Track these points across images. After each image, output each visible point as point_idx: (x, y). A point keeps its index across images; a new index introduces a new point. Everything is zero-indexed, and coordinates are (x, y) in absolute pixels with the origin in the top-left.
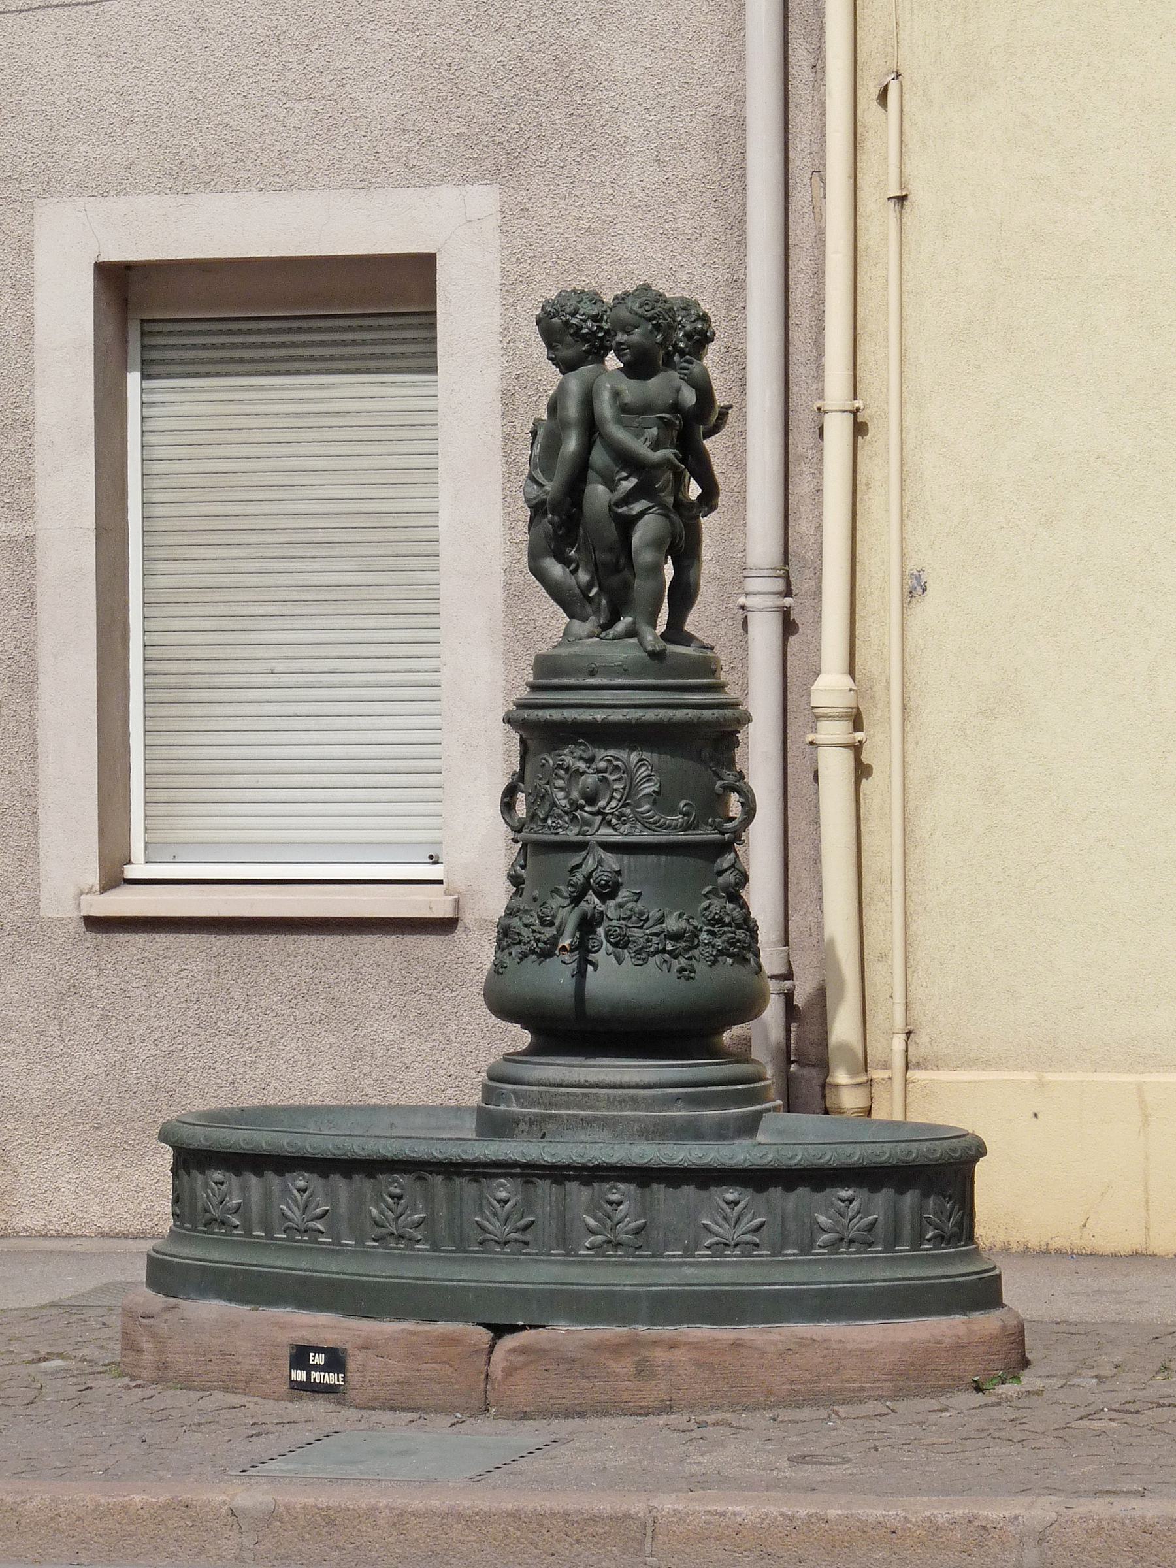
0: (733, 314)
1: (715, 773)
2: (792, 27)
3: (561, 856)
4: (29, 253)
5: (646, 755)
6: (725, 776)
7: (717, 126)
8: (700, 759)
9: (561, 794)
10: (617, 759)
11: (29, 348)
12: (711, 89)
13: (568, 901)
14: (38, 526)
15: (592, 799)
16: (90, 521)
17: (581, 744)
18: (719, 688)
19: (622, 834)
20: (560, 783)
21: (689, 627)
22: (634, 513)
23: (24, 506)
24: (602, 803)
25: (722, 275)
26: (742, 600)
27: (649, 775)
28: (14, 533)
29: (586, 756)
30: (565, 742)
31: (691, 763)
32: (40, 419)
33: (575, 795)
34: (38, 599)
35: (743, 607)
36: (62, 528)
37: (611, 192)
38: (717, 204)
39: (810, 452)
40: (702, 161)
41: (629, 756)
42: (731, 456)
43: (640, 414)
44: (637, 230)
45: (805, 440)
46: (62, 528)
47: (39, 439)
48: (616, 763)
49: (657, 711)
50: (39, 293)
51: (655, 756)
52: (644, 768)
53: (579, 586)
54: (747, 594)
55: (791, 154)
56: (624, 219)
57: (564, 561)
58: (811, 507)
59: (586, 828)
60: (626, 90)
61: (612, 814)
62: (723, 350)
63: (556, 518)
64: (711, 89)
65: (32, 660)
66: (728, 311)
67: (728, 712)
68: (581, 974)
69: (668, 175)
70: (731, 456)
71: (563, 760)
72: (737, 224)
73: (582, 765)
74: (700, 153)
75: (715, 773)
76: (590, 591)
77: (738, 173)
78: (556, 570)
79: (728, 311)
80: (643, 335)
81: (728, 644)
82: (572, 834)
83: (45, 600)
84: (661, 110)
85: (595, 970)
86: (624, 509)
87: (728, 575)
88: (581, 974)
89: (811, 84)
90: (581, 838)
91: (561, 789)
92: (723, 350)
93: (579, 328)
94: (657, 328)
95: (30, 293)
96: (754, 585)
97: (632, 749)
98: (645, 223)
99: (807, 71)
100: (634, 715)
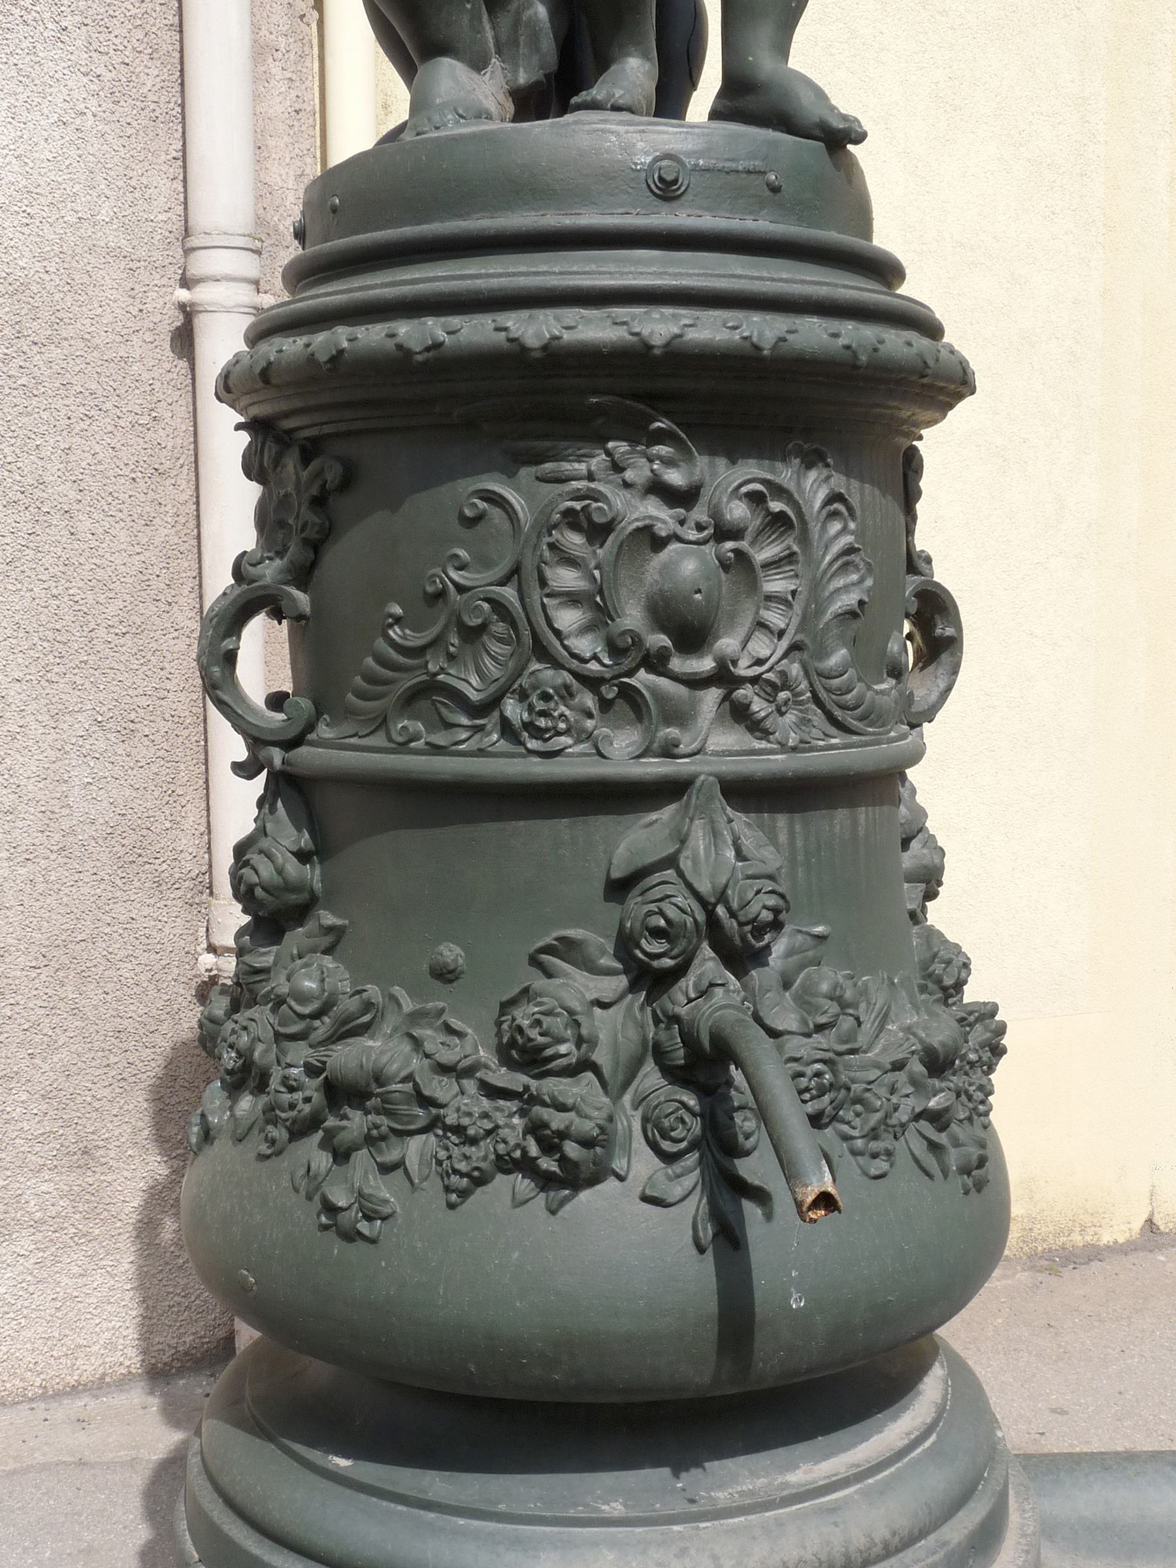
3: (601, 825)
9: (568, 618)
13: (622, 981)
15: (692, 634)
17: (660, 437)
19: (783, 747)
20: (566, 578)
24: (727, 644)
29: (675, 477)
30: (590, 430)
33: (632, 616)
39: (282, 40)
42: (139, 34)
45: (274, 19)
48: (776, 506)
58: (286, 139)
59: (672, 732)
61: (755, 680)
68: (727, 1239)
70: (139, 34)
71: (596, 496)
73: (655, 511)
82: (622, 752)
85: (769, 1216)
87: (141, 253)
88: (727, 1239)
90: (654, 768)
91: (572, 599)
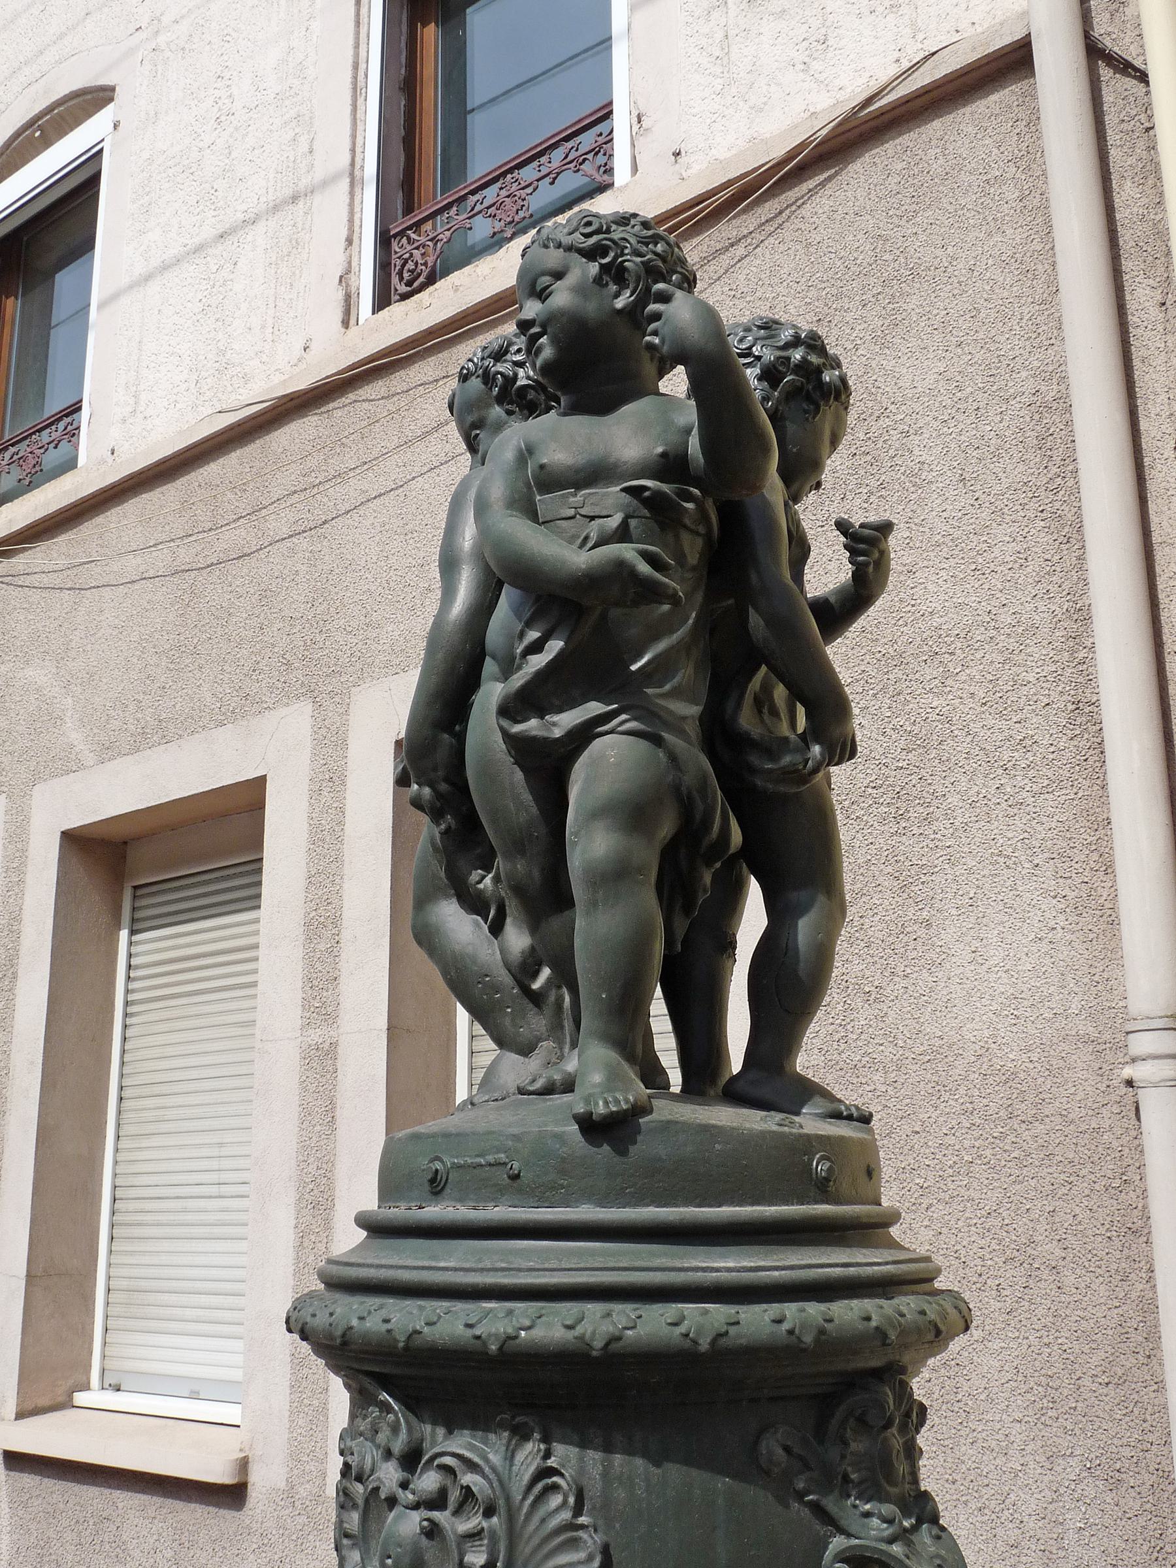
0: (1081, 655)
1: (818, 1510)
2: (1127, 265)
4: (344, 744)
5: (563, 1454)
6: (851, 1521)
7: (1037, 417)
8: (749, 1467)
10: (471, 1466)
11: (340, 840)
12: (1024, 374)
14: (341, 1031)
16: (383, 1022)
18: (871, 1229)
21: (807, 1061)
22: (557, 733)
23: (330, 1010)
25: (1060, 605)
26: (1128, 1072)
27: (571, 1526)
28: (320, 1041)
31: (724, 1483)
32: (347, 914)
34: (338, 1114)
35: (1130, 1083)
36: (360, 1031)
37: (908, 534)
38: (1044, 515)
40: (1021, 465)
41: (510, 1457)
42: (1095, 856)
43: (578, 485)
44: (942, 573)
46: (360, 1031)
47: (346, 935)
49: (672, 1310)
50: (351, 782)
51: (594, 1456)
52: (555, 1500)
53: (507, 965)
54: (1134, 1060)
55: (1143, 425)
56: (926, 563)
57: (474, 903)
60: (917, 407)
62: (1071, 707)
63: (427, 791)
64: (1024, 374)
65: (330, 1186)
66: (1073, 652)
67: (907, 1304)
69: (977, 495)
70: (1095, 856)
72: (1071, 534)
74: (1017, 456)
75: (818, 1510)
76: (535, 975)
77: (1070, 468)
78: (459, 925)
79: (1073, 652)
80: (579, 290)
81: (1115, 1144)
83: (344, 1114)
84: (961, 417)
86: (533, 723)
87: (1107, 1036)
89: (1160, 328)
92: (1071, 707)
93: (510, 380)
94: (616, 274)
95: (344, 783)
96: (1142, 1044)
97: (521, 1434)
98: (952, 562)
99: (1155, 313)
100: (597, 1323)
